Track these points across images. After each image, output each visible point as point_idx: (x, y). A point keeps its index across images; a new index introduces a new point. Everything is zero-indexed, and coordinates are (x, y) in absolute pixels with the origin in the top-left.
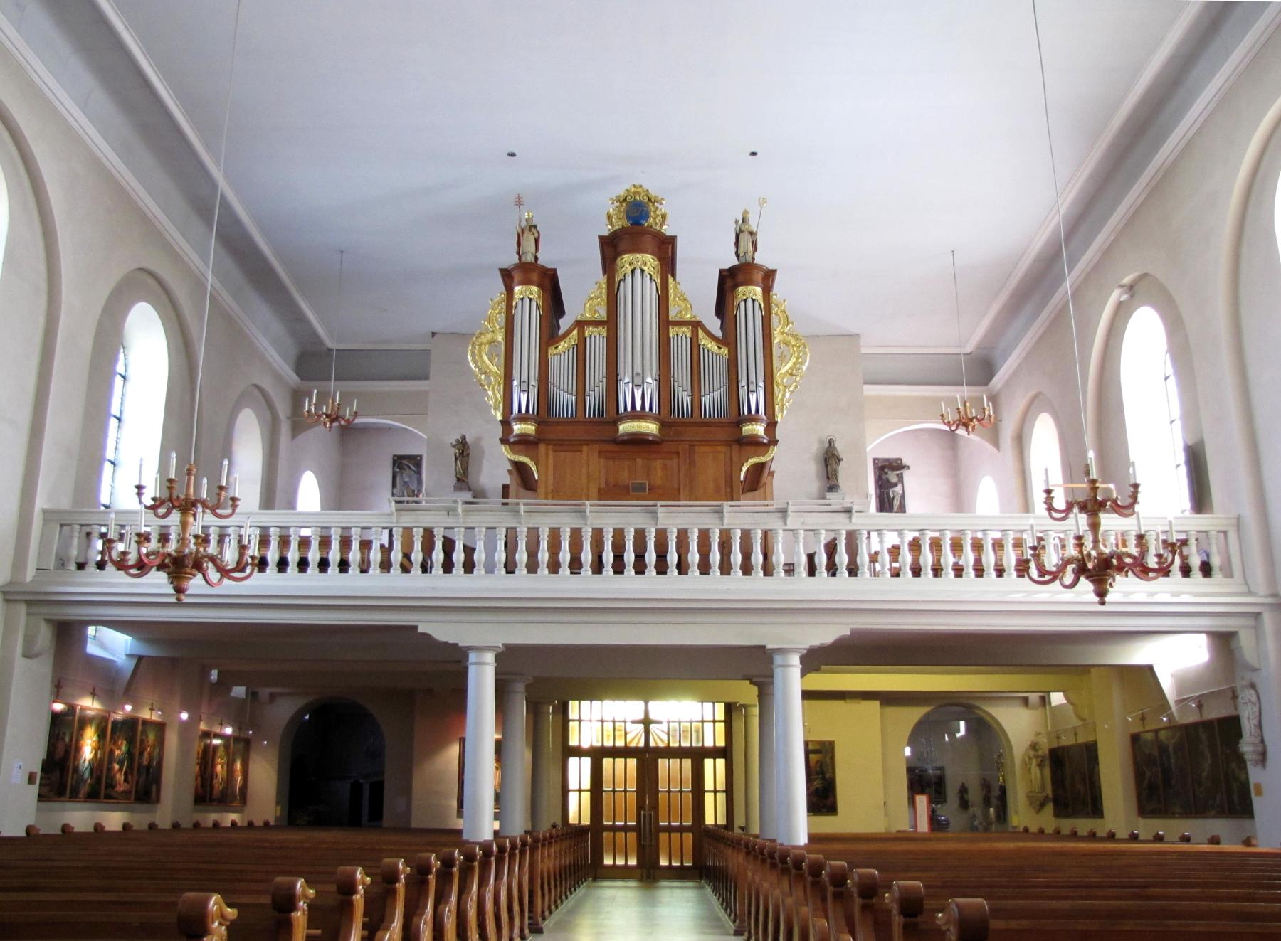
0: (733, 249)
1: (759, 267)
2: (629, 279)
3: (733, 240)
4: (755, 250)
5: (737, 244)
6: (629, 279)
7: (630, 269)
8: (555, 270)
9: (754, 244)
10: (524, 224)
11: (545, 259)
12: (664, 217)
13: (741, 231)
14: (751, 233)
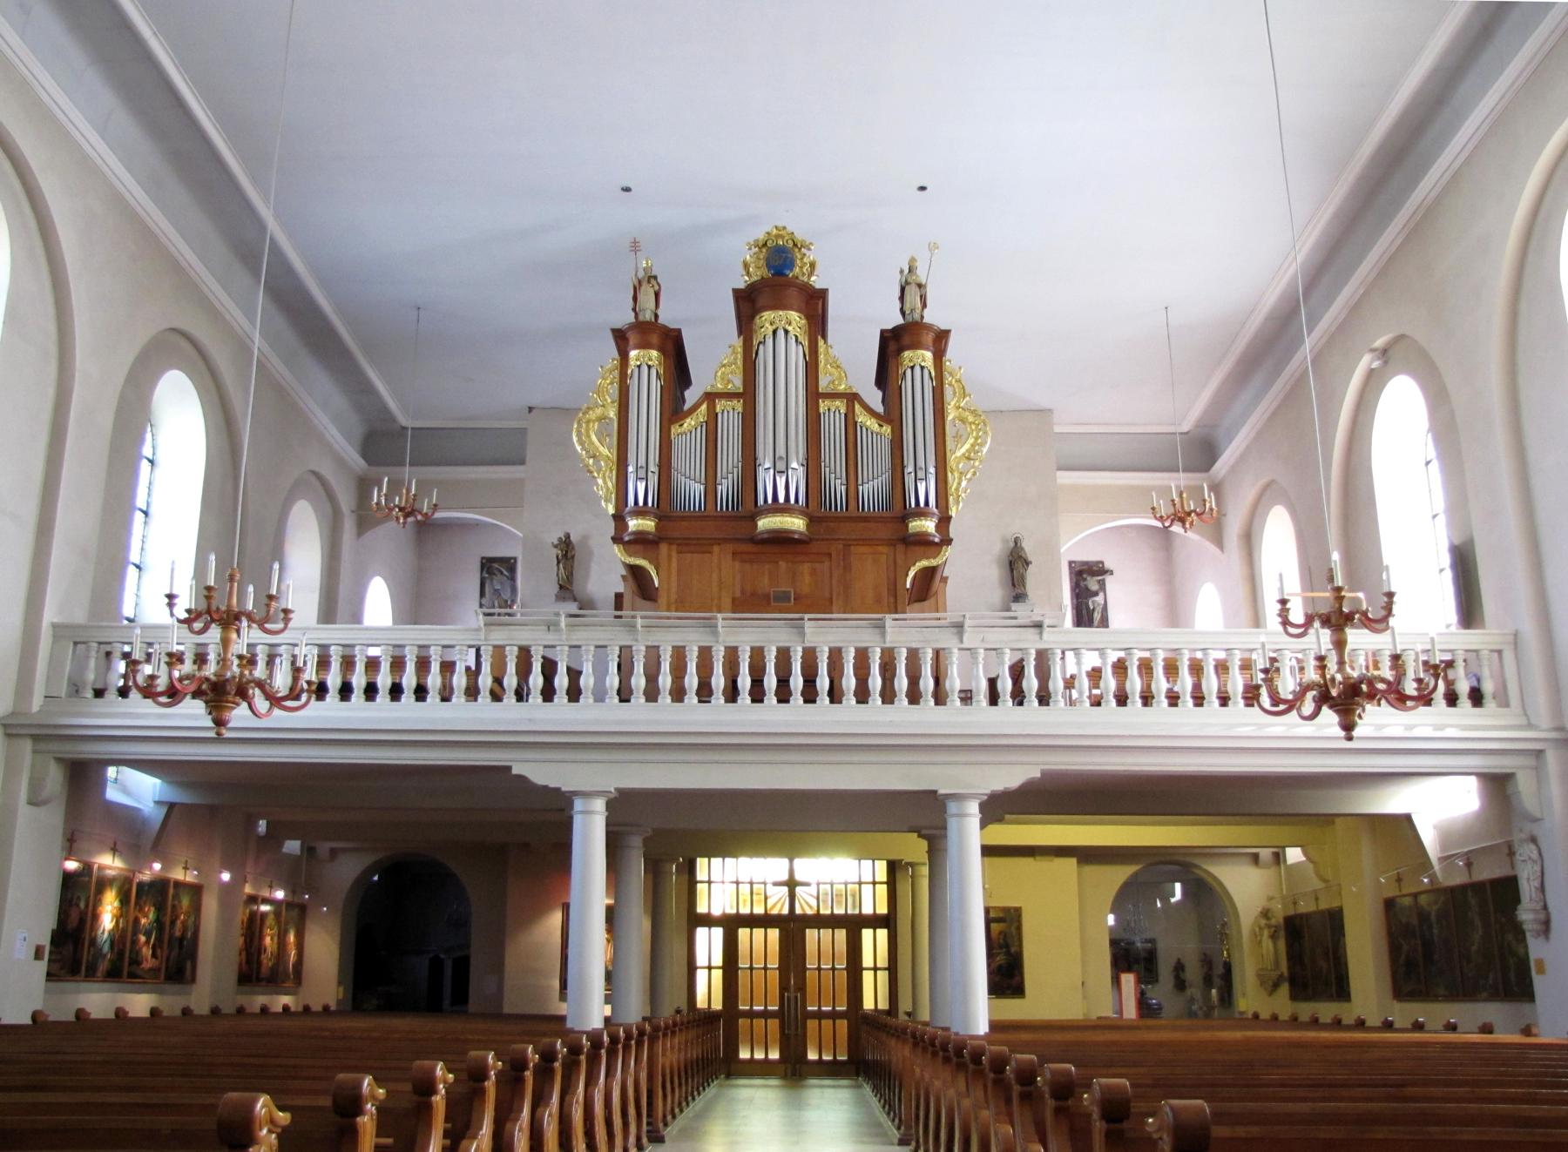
0: (898, 305)
1: (929, 327)
2: (770, 342)
3: (898, 293)
4: (924, 306)
5: (902, 298)
6: (770, 342)
7: (771, 329)
8: (679, 331)
9: (923, 299)
10: (641, 274)
11: (668, 317)
12: (813, 265)
13: (907, 283)
14: (920, 286)
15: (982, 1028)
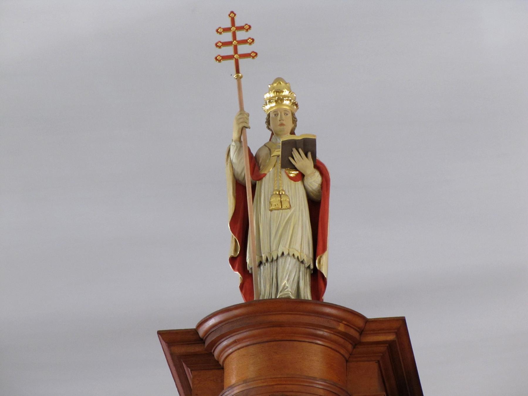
8: (399, 326)
10: (258, 138)
11: (359, 280)
15: (310, 181)
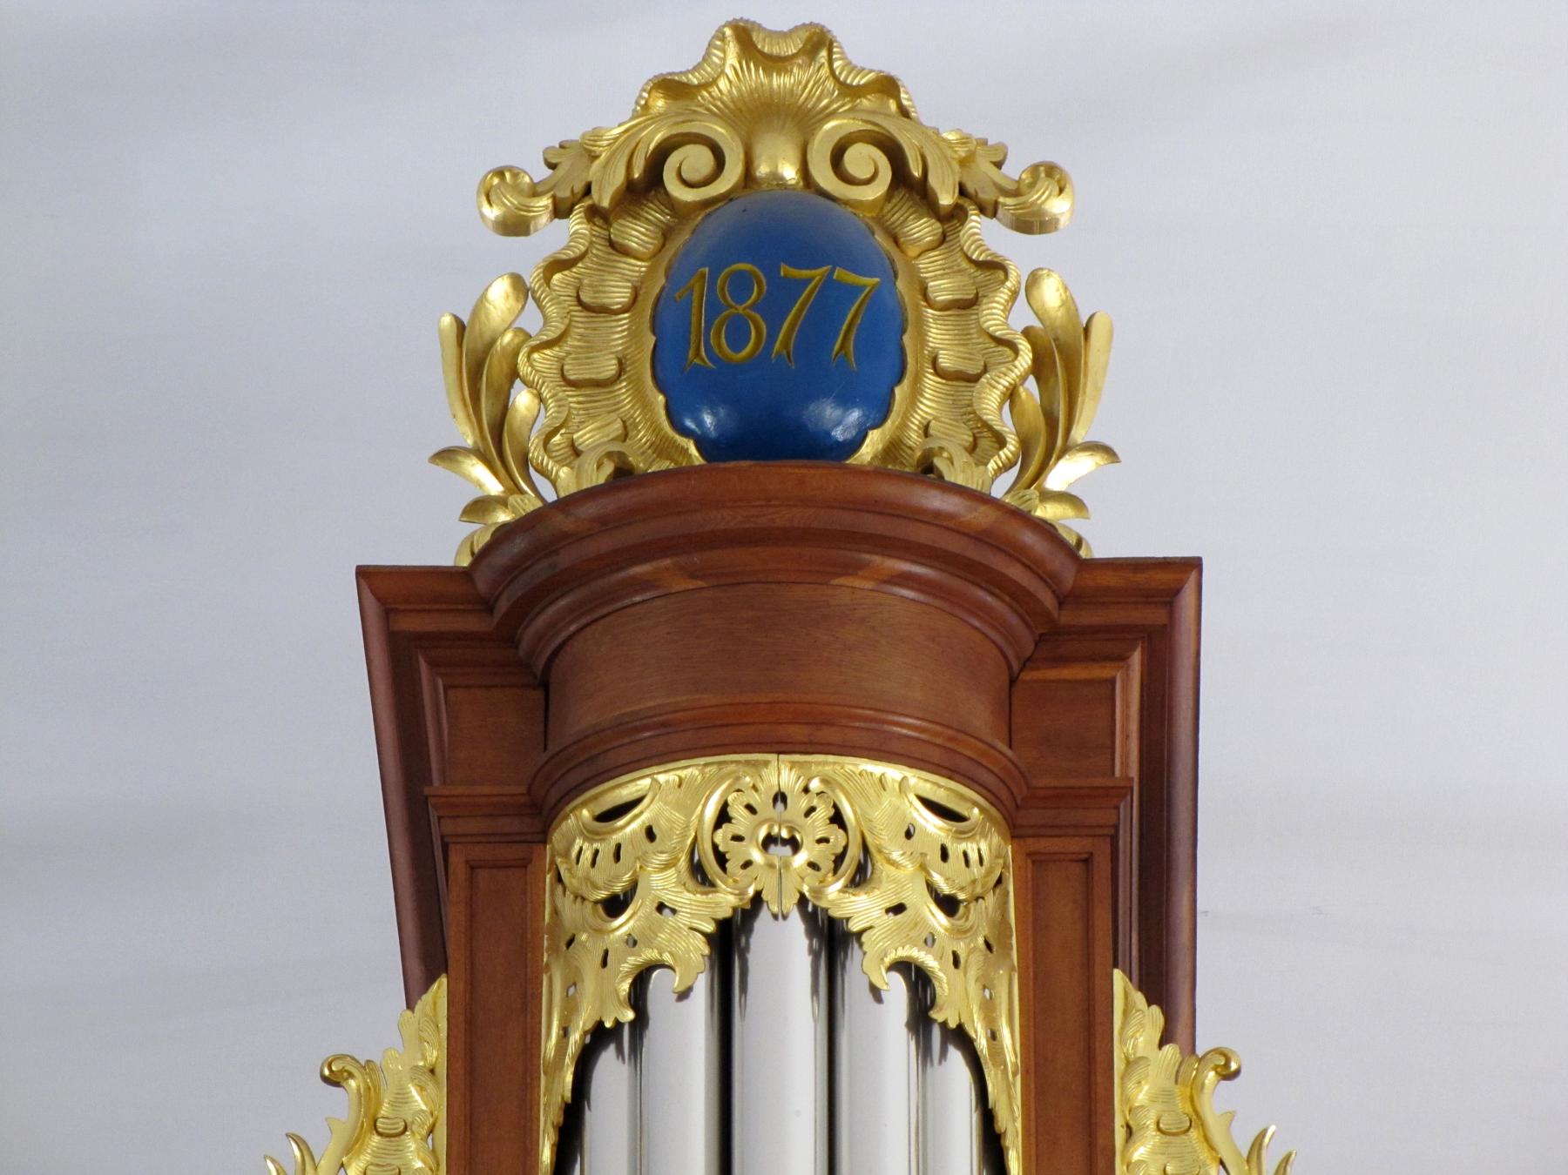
2: (685, 1027)
6: (685, 1027)
7: (699, 912)
12: (1060, 358)
